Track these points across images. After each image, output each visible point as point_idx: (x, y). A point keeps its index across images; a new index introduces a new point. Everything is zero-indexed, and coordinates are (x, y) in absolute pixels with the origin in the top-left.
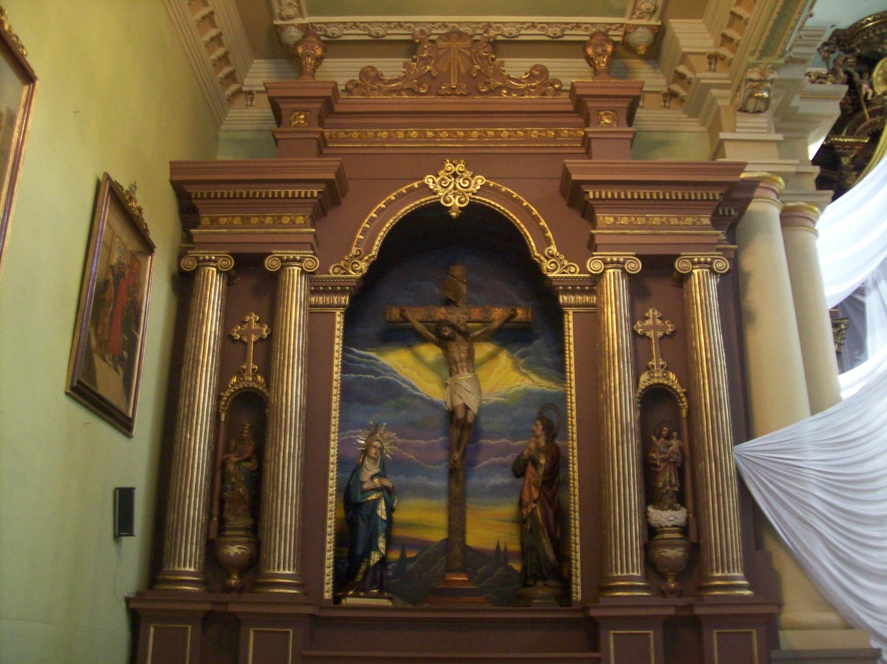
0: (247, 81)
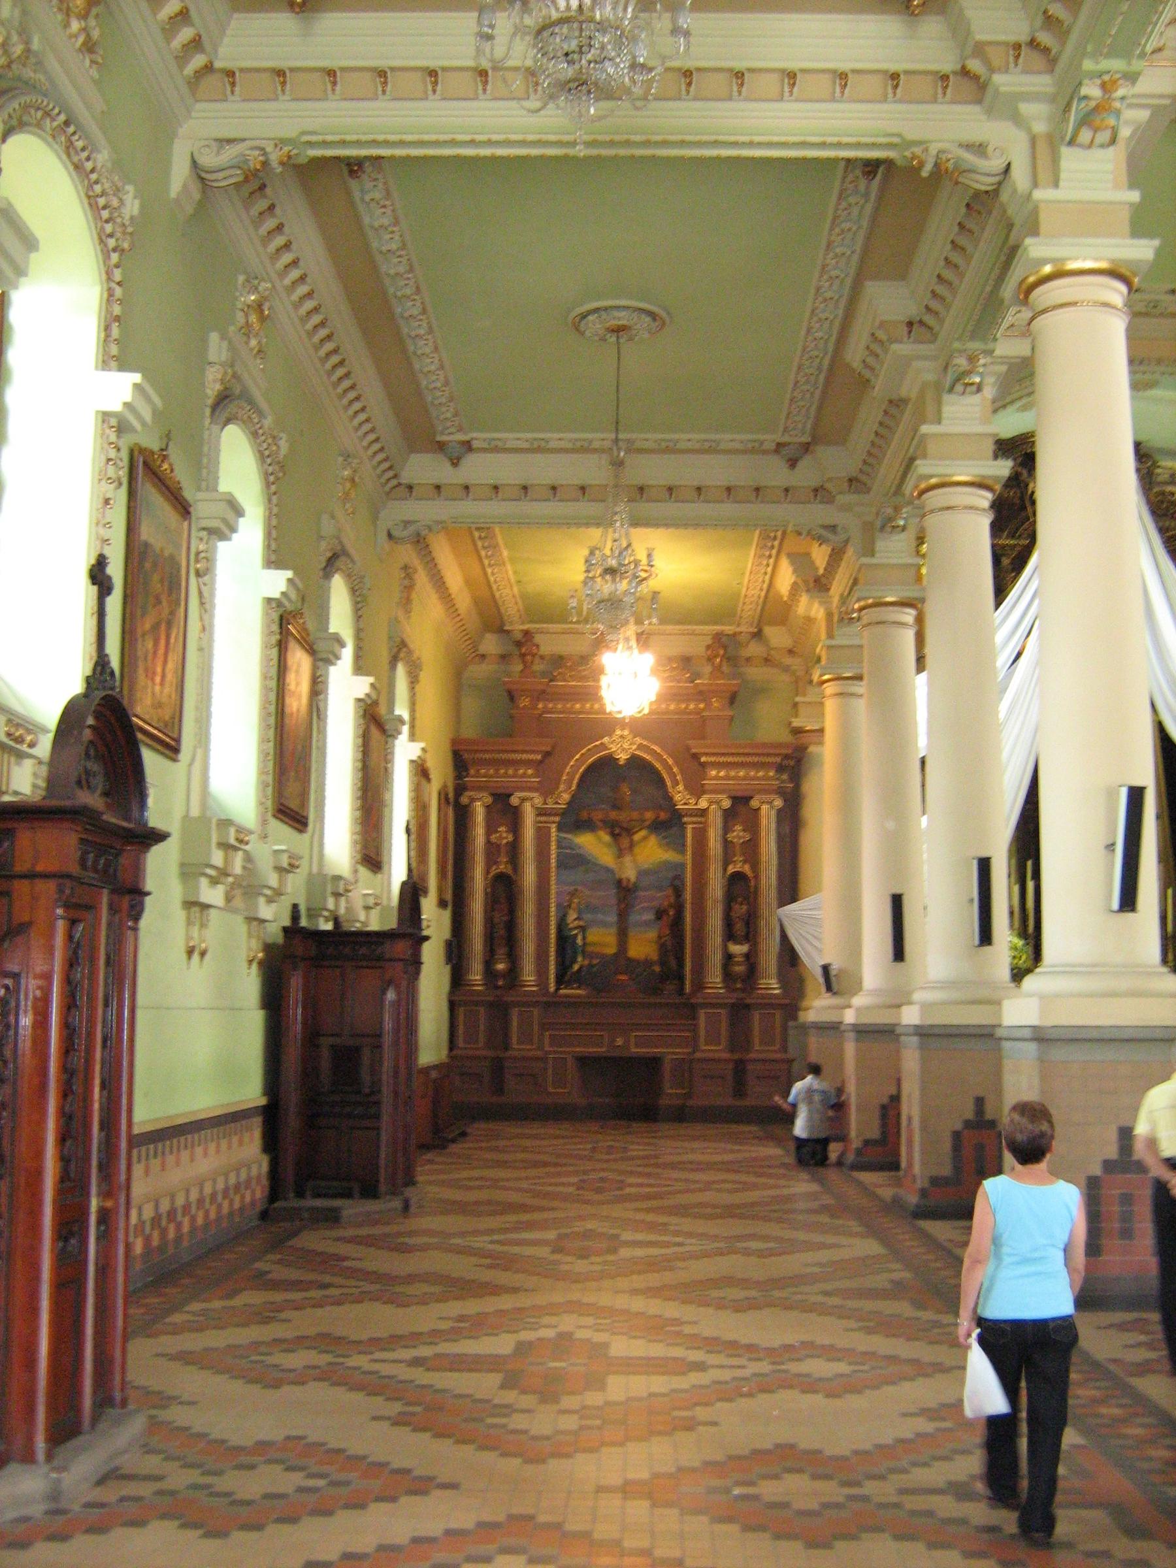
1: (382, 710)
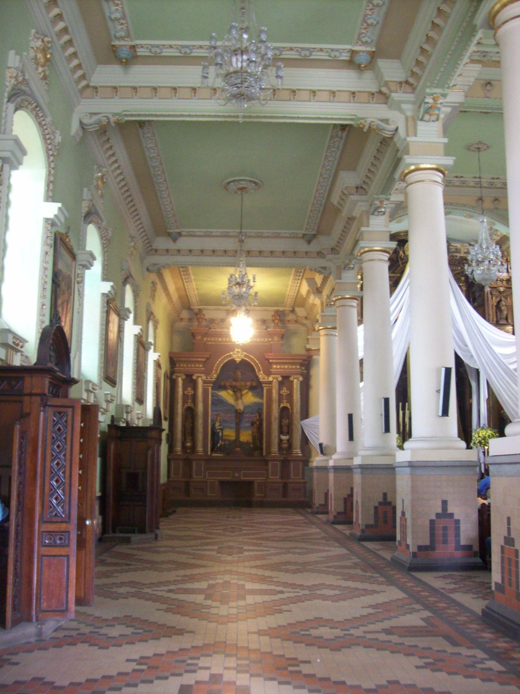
0: (93, 79)
1: (144, 339)
